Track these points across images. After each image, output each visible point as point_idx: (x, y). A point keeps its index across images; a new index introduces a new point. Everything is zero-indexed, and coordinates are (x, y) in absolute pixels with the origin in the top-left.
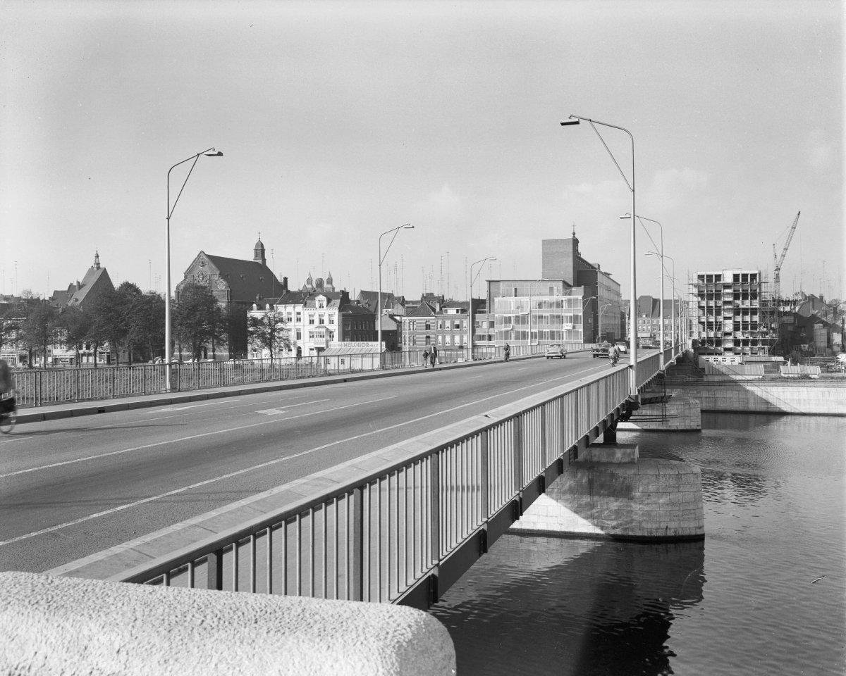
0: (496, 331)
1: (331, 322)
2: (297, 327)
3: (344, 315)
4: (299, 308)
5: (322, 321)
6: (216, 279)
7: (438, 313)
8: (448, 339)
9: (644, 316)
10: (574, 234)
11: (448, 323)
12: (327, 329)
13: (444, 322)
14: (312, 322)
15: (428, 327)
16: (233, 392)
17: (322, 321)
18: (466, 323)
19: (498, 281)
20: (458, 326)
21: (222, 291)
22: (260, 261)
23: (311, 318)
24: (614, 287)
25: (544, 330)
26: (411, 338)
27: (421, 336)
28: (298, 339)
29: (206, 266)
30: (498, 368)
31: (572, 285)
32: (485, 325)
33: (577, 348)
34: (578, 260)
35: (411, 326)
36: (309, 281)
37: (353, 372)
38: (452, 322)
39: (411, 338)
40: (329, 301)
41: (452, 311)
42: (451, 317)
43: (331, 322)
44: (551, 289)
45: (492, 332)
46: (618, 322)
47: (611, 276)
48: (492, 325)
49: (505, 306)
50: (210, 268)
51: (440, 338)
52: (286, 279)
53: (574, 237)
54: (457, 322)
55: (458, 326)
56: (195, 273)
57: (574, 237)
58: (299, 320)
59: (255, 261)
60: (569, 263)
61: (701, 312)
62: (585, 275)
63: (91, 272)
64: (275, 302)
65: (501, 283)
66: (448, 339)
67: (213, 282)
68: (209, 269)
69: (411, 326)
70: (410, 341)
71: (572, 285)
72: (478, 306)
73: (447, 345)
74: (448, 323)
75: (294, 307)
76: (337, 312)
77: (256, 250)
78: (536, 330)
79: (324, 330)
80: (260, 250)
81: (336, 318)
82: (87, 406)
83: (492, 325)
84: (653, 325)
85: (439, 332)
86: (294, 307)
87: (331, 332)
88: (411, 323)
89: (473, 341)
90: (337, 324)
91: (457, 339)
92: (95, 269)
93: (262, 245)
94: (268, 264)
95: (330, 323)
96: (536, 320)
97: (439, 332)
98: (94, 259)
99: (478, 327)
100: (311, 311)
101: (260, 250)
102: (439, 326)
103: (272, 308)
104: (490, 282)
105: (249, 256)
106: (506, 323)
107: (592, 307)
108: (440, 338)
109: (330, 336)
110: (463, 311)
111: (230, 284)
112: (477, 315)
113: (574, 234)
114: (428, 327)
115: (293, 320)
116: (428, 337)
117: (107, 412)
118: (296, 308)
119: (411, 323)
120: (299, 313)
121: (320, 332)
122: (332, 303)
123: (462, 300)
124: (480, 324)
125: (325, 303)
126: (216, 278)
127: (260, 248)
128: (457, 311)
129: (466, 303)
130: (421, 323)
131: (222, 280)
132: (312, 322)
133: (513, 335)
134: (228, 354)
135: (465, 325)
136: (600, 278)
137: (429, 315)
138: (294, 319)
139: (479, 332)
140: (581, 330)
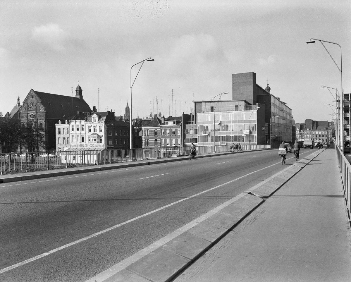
0: (199, 136)
1: (101, 131)
2: (77, 134)
3: (107, 126)
4: (83, 122)
5: (95, 130)
6: (39, 105)
7: (163, 124)
8: (168, 141)
9: (308, 130)
10: (268, 85)
11: (168, 131)
12: (98, 135)
13: (166, 130)
14: (90, 131)
15: (156, 133)
16: (115, 167)
17: (95, 130)
18: (180, 131)
19: (201, 102)
20: (174, 133)
21: (42, 112)
22: (78, 97)
23: (90, 129)
24: (287, 110)
25: (230, 135)
26: (146, 141)
27: (152, 139)
28: (82, 142)
29: (34, 98)
30: (265, 152)
31: (252, 104)
32: (192, 132)
33: (253, 148)
34: (257, 88)
35: (146, 133)
36: (151, 115)
37: (86, 165)
38: (171, 131)
39: (146, 141)
40: (99, 118)
41: (171, 123)
42: (170, 127)
43: (101, 131)
44: (237, 106)
45: (196, 136)
46: (290, 131)
47: (286, 104)
48: (196, 132)
49: (204, 118)
50: (36, 99)
51: (163, 140)
52: (94, 107)
53: (268, 86)
54: (174, 130)
55: (174, 133)
56: (29, 102)
57: (268, 86)
58: (83, 129)
59: (76, 97)
60: (251, 88)
61: (346, 122)
62: (262, 98)
63: (15, 107)
64: (71, 119)
65: (203, 104)
66: (168, 141)
67: (38, 107)
68: (36, 100)
69: (146, 133)
70: (145, 143)
71: (252, 104)
72: (187, 119)
73: (168, 145)
74: (168, 131)
75: (75, 122)
76: (104, 124)
77: (77, 91)
78: (225, 135)
79: (96, 136)
80: (79, 91)
81: (103, 128)
82: (127, 164)
83: (196, 132)
84: (313, 135)
85: (162, 137)
86: (75, 122)
87: (101, 137)
88: (146, 131)
89: (184, 143)
90: (104, 132)
91: (174, 141)
92: (17, 106)
93: (80, 88)
94: (84, 98)
95: (100, 131)
96: (225, 128)
97: (162, 137)
98: (17, 101)
99: (188, 133)
100: (90, 125)
101: (79, 91)
102: (163, 133)
103: (68, 123)
104: (196, 103)
105: (73, 94)
106: (205, 130)
107: (264, 117)
108: (163, 140)
109: (100, 140)
110: (178, 123)
111: (46, 109)
112: (187, 126)
113: (268, 85)
114: (156, 133)
115: (80, 129)
116: (156, 140)
117: (5, 183)
118: (82, 122)
119: (146, 131)
120: (83, 126)
121: (94, 137)
122: (101, 119)
123: (178, 116)
124: (189, 131)
125: (97, 119)
126: (39, 105)
127: (79, 90)
128: (174, 123)
129: (180, 118)
130: (152, 131)
131: (42, 106)
132: (90, 131)
133: (210, 139)
134: (45, 150)
135: (178, 132)
136: (273, 100)
137: (157, 125)
138: (75, 129)
139: (188, 137)
140: (256, 135)
